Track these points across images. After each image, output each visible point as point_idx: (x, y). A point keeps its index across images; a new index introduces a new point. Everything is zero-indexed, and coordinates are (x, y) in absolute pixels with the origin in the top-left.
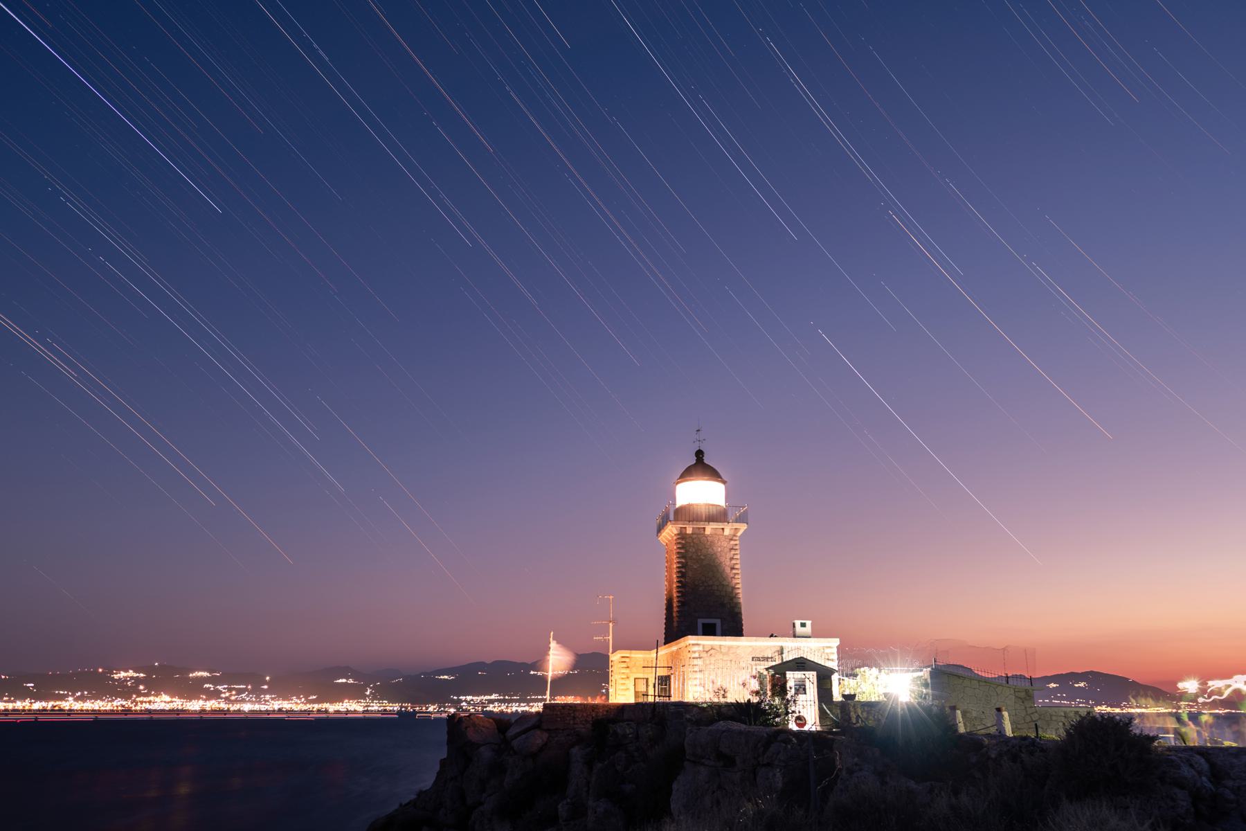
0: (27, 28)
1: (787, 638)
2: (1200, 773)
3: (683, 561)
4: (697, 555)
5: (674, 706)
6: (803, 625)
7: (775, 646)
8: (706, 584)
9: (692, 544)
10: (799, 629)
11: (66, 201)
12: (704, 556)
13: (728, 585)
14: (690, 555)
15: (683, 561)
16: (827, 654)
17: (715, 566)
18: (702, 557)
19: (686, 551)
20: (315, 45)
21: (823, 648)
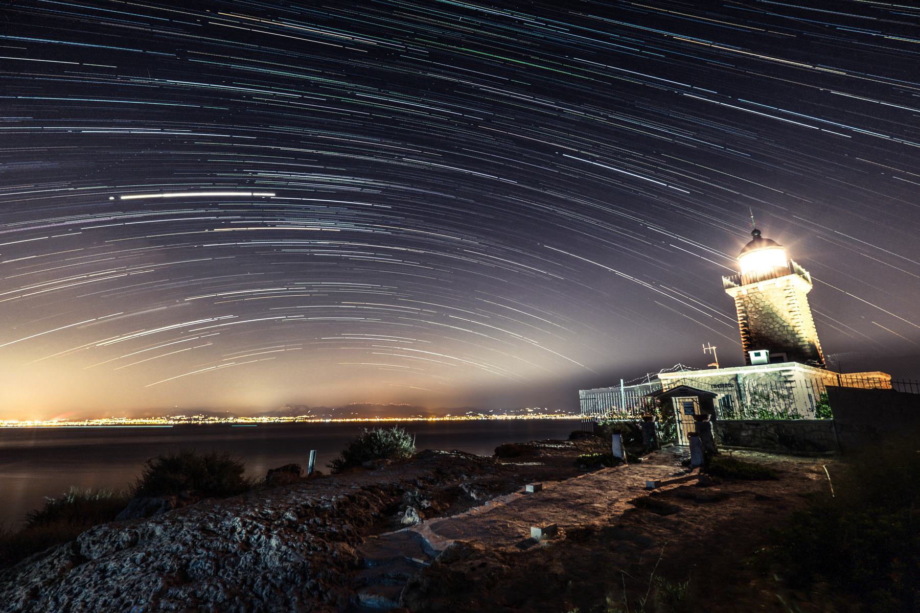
0: (543, 67)
1: (739, 367)
2: (569, 485)
3: (744, 315)
4: (756, 308)
5: (753, 424)
6: (758, 355)
7: (730, 375)
8: (767, 328)
9: (750, 301)
10: (753, 358)
11: (423, 151)
12: (761, 307)
13: (789, 326)
14: (749, 309)
15: (744, 315)
16: (785, 377)
17: (774, 313)
18: (760, 309)
19: (746, 307)
20: (666, 33)
21: (780, 372)
